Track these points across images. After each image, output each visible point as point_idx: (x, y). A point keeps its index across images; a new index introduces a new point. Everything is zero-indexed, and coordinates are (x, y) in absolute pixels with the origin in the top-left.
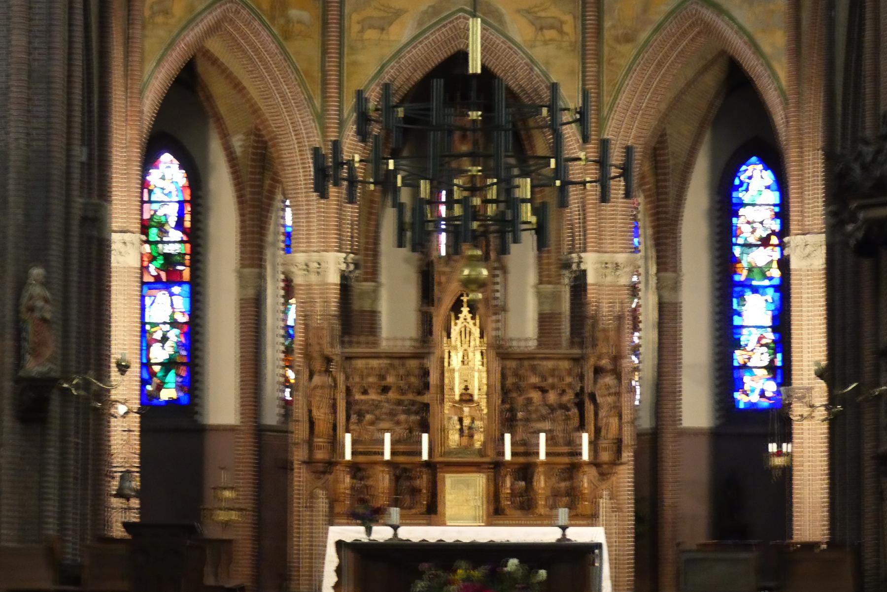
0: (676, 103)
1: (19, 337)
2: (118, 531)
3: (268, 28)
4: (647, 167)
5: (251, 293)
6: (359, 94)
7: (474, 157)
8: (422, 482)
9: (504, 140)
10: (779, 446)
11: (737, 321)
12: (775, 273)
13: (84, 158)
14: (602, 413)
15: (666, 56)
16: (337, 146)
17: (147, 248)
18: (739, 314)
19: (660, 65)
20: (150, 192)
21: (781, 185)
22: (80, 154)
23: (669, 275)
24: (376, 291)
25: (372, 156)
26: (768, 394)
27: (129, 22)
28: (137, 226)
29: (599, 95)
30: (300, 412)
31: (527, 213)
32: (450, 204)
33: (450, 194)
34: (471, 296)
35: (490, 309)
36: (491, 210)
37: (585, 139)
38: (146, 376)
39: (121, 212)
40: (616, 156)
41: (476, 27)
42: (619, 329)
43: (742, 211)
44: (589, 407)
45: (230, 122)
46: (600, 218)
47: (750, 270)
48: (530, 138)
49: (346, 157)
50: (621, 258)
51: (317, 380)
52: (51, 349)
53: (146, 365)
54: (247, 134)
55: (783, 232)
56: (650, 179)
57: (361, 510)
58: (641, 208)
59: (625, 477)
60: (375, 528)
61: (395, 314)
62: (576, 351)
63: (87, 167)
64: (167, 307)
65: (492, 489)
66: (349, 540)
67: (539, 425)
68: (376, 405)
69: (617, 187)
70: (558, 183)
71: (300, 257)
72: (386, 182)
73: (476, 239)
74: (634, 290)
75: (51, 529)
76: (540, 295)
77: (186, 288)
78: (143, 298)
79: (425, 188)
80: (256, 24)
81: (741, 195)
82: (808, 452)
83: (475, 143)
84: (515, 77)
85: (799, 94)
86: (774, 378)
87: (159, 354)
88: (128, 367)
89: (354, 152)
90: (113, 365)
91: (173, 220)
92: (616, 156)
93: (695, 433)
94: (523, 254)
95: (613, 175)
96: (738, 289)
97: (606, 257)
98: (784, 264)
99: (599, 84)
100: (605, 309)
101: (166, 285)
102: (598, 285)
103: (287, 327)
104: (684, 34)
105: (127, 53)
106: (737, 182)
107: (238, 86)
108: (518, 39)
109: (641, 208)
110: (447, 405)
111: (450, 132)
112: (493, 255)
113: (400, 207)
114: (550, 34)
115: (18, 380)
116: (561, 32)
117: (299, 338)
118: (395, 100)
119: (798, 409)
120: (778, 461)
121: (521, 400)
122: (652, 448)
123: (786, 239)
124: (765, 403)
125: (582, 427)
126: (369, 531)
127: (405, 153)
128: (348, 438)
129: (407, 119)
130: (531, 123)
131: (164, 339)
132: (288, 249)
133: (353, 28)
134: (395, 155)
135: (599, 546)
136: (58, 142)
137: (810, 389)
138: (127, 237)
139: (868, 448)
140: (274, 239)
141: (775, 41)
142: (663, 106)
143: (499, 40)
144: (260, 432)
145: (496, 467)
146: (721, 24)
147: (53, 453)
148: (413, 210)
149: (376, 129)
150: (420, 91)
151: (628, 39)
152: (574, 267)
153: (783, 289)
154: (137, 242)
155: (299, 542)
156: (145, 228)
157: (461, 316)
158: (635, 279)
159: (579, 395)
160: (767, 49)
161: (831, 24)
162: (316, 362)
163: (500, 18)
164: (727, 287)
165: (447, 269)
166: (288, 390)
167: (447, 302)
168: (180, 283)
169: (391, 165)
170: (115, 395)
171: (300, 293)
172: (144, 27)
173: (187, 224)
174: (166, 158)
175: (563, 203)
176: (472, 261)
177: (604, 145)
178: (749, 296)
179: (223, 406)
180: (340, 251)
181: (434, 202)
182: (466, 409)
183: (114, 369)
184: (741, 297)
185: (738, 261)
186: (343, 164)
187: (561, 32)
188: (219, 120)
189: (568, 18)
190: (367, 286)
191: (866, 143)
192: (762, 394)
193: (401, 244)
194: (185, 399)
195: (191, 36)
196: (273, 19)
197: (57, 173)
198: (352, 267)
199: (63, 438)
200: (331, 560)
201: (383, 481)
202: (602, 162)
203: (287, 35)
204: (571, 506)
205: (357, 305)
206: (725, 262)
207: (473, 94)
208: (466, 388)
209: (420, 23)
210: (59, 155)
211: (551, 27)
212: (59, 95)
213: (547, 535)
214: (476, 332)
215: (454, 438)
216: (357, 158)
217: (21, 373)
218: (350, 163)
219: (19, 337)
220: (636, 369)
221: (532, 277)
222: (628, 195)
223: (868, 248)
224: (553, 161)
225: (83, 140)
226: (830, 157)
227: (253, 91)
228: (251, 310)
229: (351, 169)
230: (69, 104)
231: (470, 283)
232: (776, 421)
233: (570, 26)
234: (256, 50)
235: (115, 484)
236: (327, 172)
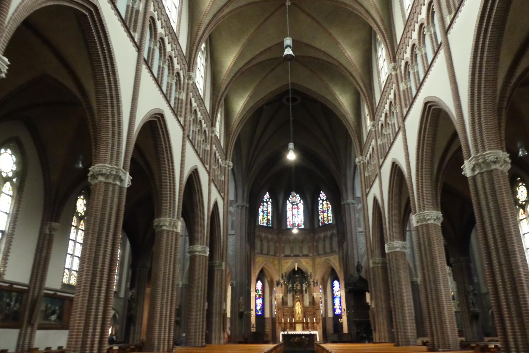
1: (239, 306)
59: (321, 324)
64: (259, 301)
71: (277, 294)
82: (344, 320)
93: (330, 318)
95: (520, 218)
119: (343, 314)
122: (325, 320)
140: (273, 292)
145: (303, 323)
164: (333, 297)
174: (259, 282)
179: (267, 315)
201: (288, 325)
205: (285, 300)
215: (297, 319)
219: (239, 306)
232: (340, 316)
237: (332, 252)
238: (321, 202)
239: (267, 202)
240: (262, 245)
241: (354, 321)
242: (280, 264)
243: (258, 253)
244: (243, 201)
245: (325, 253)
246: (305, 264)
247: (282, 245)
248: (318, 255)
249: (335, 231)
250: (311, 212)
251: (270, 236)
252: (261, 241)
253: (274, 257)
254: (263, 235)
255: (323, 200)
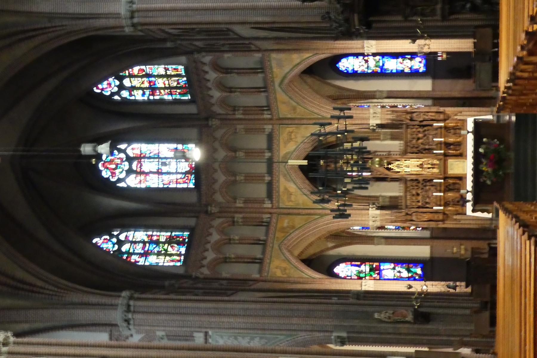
0: (317, 92)
2: (469, 290)
3: (291, 234)
4: (339, 102)
5: (383, 240)
6: (314, 202)
7: (336, 162)
8: (451, 181)
9: (331, 152)
10: (439, 56)
11: (394, 71)
12: (378, 58)
13: (336, 298)
14: (427, 117)
15: (301, 96)
16: (332, 210)
17: (367, 278)
18: (392, 70)
19: (304, 98)
20: (348, 276)
21: (346, 56)
22: (335, 300)
23: (378, 94)
24: (382, 196)
25: (336, 198)
26: (420, 60)
27: (288, 282)
28: (360, 281)
29: (314, 119)
30: (426, 225)
31: (357, 144)
32: (352, 171)
33: (349, 171)
34: (386, 164)
35: (389, 158)
36: (355, 157)
37: (330, 124)
38: (412, 279)
39: (355, 286)
40: (337, 113)
41: (291, 162)
42: (396, 112)
43: (356, 69)
44: (425, 123)
45: (323, 247)
46: (358, 119)
47: (376, 66)
48: (329, 143)
49: (336, 207)
50: (371, 111)
51: (414, 218)
52: (403, 311)
53: (409, 278)
54: (328, 241)
55: (363, 55)
56: (344, 101)
57: (461, 203)
58: (354, 104)
59: (449, 110)
60: (467, 199)
61: (392, 190)
62: (404, 126)
63: (339, 297)
64: (388, 271)
65: (454, 157)
66: (472, 208)
67: (431, 140)
68: (423, 196)
69: (347, 113)
70: (346, 134)
71: (371, 223)
72: (345, 193)
73: (365, 162)
74: (383, 107)
75: (468, 312)
76: (384, 140)
77: (381, 264)
78: (385, 279)
79: (347, 180)
80: (289, 238)
81: (350, 71)
82: (441, 46)
83: (331, 162)
84: (308, 148)
85: (314, 49)
86: (415, 58)
87: (405, 274)
88: (410, 285)
89: (334, 205)
90: (409, 290)
91: (357, 268)
92: (337, 113)
93: (433, 84)
94: (370, 145)
96: (383, 71)
97: (371, 116)
98: (374, 55)
99: (310, 119)
100: (390, 117)
101: (380, 271)
102: (381, 119)
103: (396, 229)
104: (293, 89)
105: (299, 283)
106: (346, 71)
107: (311, 245)
108: (294, 147)
109: (354, 104)
110: (423, 173)
111: (327, 171)
112: (370, 156)
113: (354, 188)
114: (293, 136)
115: (415, 323)
116: (292, 132)
117: (399, 224)
118: (316, 190)
119: (426, 50)
120: (445, 56)
121: (422, 146)
122: (439, 100)
123: (366, 54)
124: (424, 61)
125: (432, 125)
126: (469, 201)
127: (334, 186)
128: (434, 208)
129: (323, 186)
130: (324, 142)
131: (399, 272)
132: (368, 228)
133: (290, 204)
134: (335, 190)
135: (475, 119)
136: (330, 307)
137: (419, 45)
138: (363, 284)
139: (439, 24)
140: (364, 233)
141: (296, 58)
142: (318, 97)
143: (295, 154)
144: (433, 238)
145: (445, 155)
146: (289, 77)
147: (440, 311)
148: (355, 184)
149: (326, 197)
150: (313, 181)
151: (294, 109)
152: (375, 128)
153: (383, 55)
154: (365, 281)
155: (473, 225)
156: (360, 278)
157: (392, 168)
158: (379, 107)
159: (420, 126)
160: (298, 61)
161: (290, 38)
162: (408, 219)
163: (287, 153)
164: (382, 74)
165: (375, 171)
166: (418, 229)
167: (387, 172)
168: (380, 266)
169: (339, 192)
170: (419, 290)
171: (383, 224)
172: (290, 277)
173: (359, 263)
175: (352, 131)
176: (373, 163)
177: (333, 117)
178: (385, 67)
179: (423, 251)
180: (369, 210)
181: (351, 177)
182: (425, 166)
183: (411, 290)
184: (385, 70)
185: (373, 71)
186: (339, 209)
187: (292, 132)
188: (322, 251)
189: (288, 129)
190: (381, 200)
191: (331, 26)
192: (420, 62)
193: (366, 188)
194: (421, 265)
195: (294, 261)
196: (287, 232)
197: (342, 308)
198: (374, 206)
199: (435, 307)
200: (479, 214)
202: (339, 118)
203: (293, 227)
204: (460, 129)
205: (387, 203)
206: (374, 75)
207: (314, 163)
208: (418, 166)
209: (289, 181)
210: (335, 307)
211: (290, 135)
212: (312, 307)
213: (470, 138)
214: (398, 163)
215: (436, 171)
216: (337, 204)
217: (412, 321)
218: (338, 206)
220: (411, 106)
221: (378, 142)
222: (350, 109)
223: (369, 25)
224: (338, 136)
225: (330, 299)
226: (336, 38)
227: (312, 239)
228: (389, 240)
229: (341, 205)
230: (317, 303)
231: (381, 165)
232: (430, 58)
233: (290, 129)
234: (298, 238)
235: (452, 290)
236: (342, 214)
237: (261, 69)
238: (125, 94)
239: (120, 243)
240: (240, 260)
241: (444, 18)
242: (291, 212)
243: (260, 271)
244: (113, 306)
245: (265, 89)
246: (293, 148)
247: (239, 204)
248: (269, 108)
249: (208, 58)
250: (152, 121)
251: (215, 237)
252: (226, 260)
253: (272, 228)
254: (211, 256)
255: (121, 87)
